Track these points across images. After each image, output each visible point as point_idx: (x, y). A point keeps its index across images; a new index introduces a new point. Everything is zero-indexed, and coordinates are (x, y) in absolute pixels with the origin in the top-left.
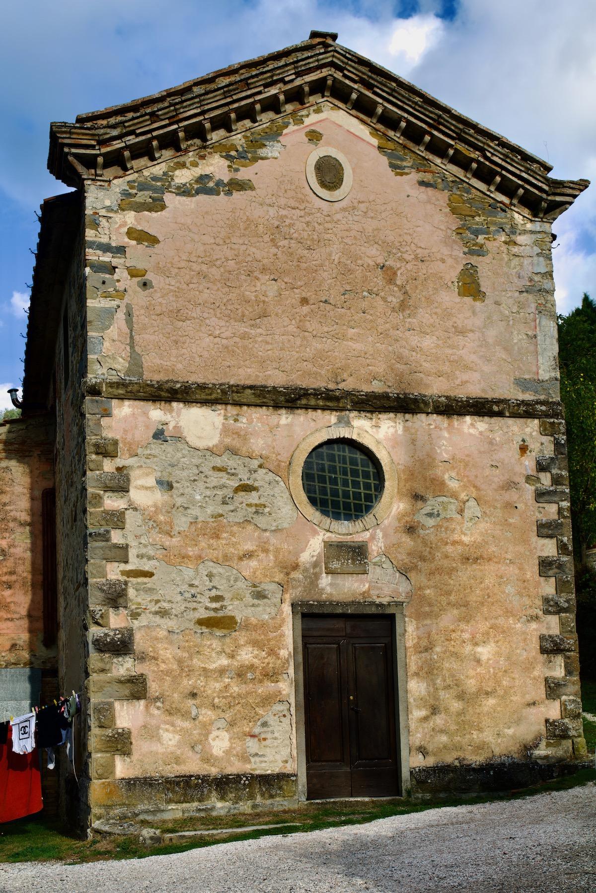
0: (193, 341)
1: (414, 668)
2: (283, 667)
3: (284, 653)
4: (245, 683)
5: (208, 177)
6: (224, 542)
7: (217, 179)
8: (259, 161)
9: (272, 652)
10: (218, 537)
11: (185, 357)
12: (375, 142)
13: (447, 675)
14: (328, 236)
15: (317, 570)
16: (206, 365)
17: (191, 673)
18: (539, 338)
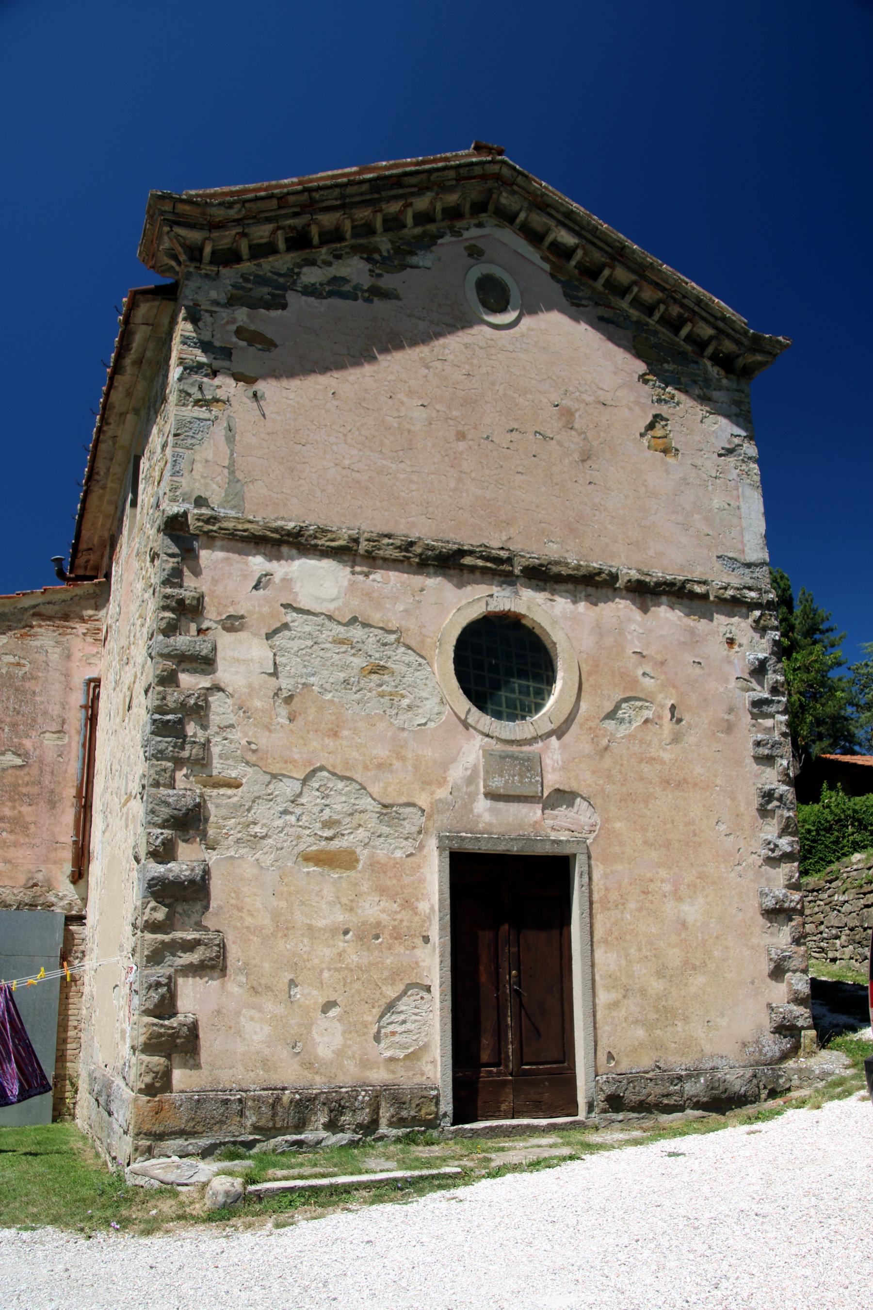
0: (314, 470)
1: (601, 932)
2: (422, 926)
3: (423, 906)
4: (368, 949)
5: (345, 281)
6: (344, 743)
7: (355, 282)
8: (408, 269)
9: (408, 904)
10: (336, 734)
11: (302, 489)
12: (547, 267)
13: (643, 943)
14: (492, 362)
15: (472, 788)
16: (330, 503)
17: (290, 932)
18: (742, 510)
